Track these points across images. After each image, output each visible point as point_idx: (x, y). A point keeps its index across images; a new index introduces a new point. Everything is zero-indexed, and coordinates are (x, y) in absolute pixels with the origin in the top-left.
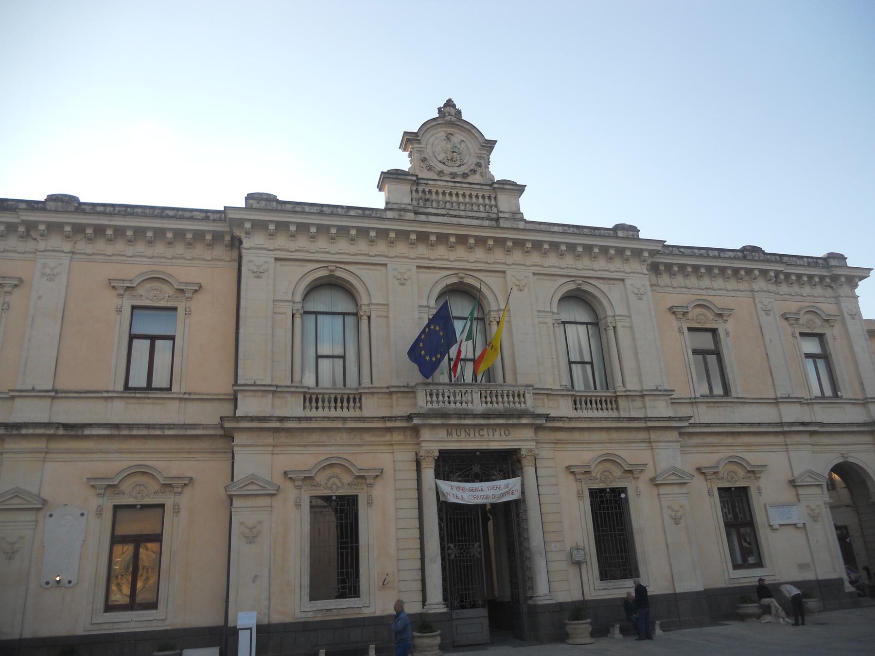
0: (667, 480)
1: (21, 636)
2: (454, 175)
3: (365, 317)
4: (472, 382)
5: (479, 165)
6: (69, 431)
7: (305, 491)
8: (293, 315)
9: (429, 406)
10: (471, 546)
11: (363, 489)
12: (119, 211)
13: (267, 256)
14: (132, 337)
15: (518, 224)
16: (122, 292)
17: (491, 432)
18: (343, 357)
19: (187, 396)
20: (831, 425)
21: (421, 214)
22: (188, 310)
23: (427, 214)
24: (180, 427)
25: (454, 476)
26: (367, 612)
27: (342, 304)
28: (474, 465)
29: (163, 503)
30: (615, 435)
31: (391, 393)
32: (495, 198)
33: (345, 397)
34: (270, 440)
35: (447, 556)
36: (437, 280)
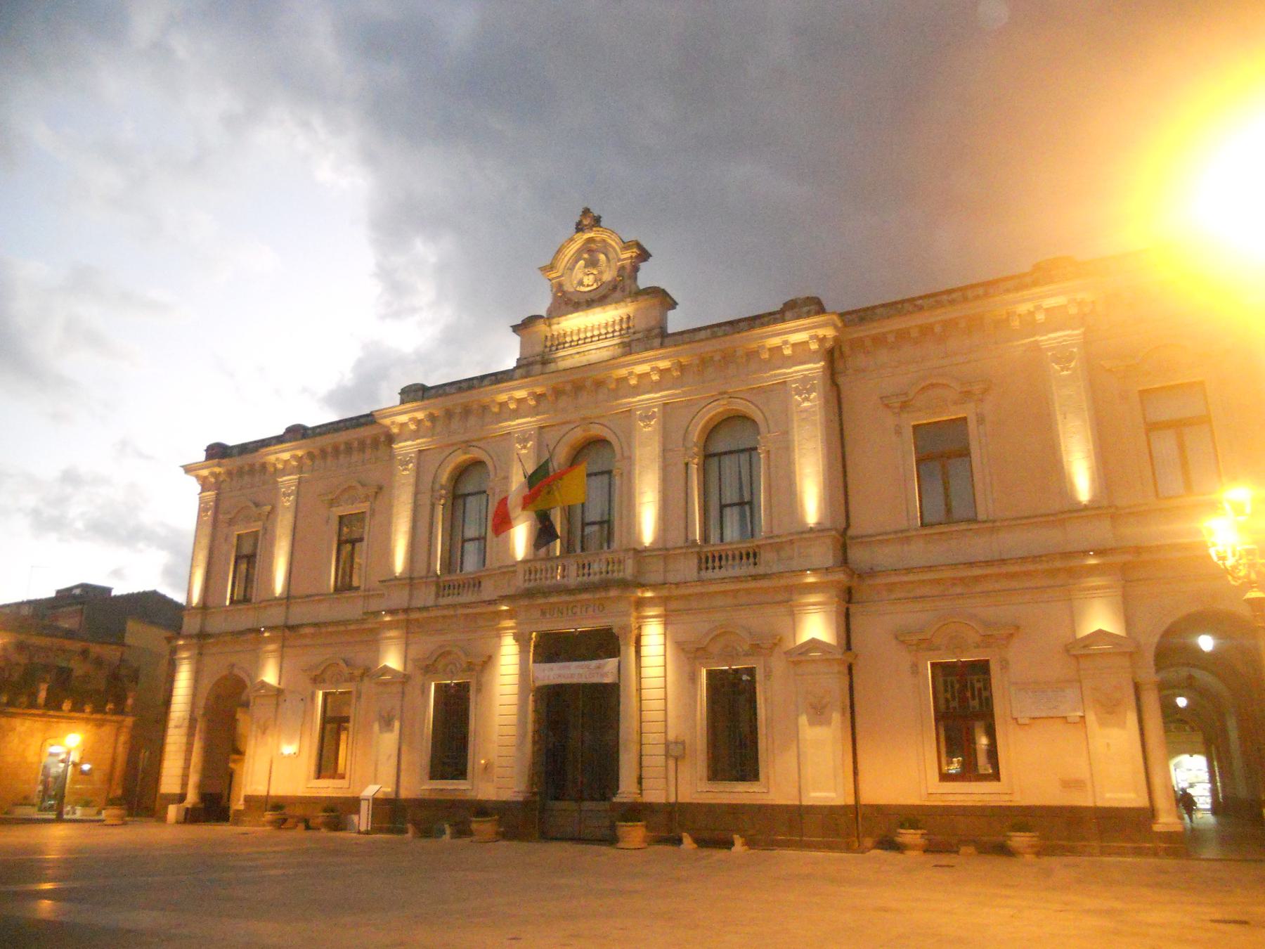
9: (580, 579)
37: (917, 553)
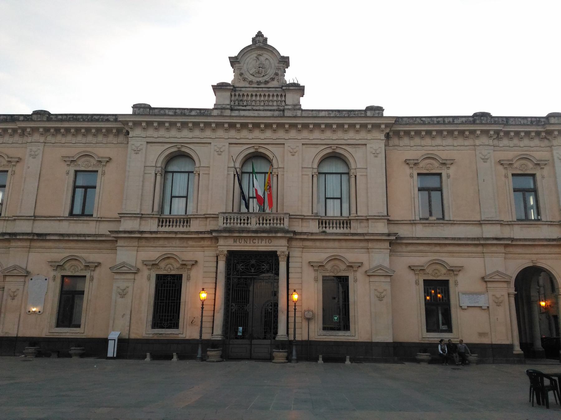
0: (375, 273)
1: (17, 335)
2: (259, 83)
3: (275, 175)
4: (259, 212)
5: (277, 74)
6: (39, 237)
7: (153, 271)
8: (313, 176)
9: (225, 225)
10: (245, 306)
11: (185, 271)
12: (70, 118)
13: (142, 141)
14: (75, 187)
15: (297, 113)
16: (69, 163)
17: (260, 241)
18: (341, 199)
19: (100, 219)
20: (524, 240)
21: (235, 110)
22: (103, 172)
23: (239, 110)
24: (93, 236)
25: (239, 265)
26: (181, 337)
27: (341, 168)
28: (252, 260)
29: (348, 275)
30: (344, 244)
31: (206, 218)
32: (285, 96)
33: (342, 221)
34: (136, 244)
35: (230, 310)
36: (241, 152)
37: (421, 231)
